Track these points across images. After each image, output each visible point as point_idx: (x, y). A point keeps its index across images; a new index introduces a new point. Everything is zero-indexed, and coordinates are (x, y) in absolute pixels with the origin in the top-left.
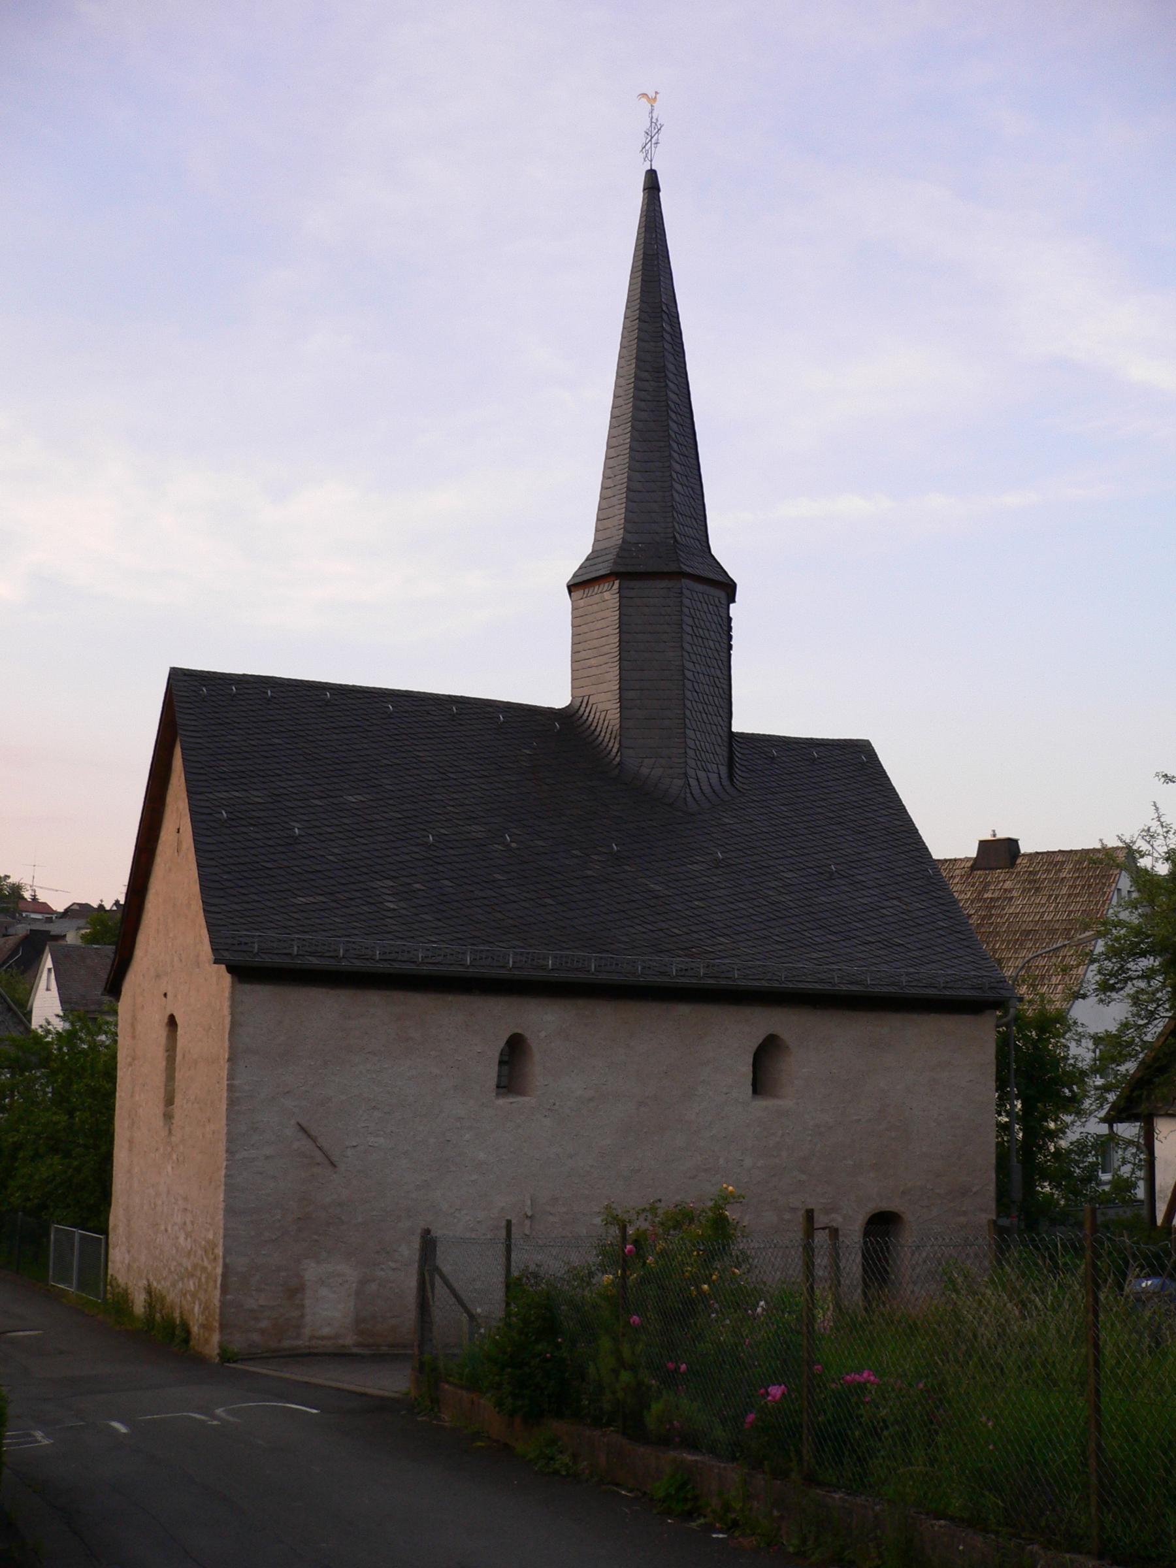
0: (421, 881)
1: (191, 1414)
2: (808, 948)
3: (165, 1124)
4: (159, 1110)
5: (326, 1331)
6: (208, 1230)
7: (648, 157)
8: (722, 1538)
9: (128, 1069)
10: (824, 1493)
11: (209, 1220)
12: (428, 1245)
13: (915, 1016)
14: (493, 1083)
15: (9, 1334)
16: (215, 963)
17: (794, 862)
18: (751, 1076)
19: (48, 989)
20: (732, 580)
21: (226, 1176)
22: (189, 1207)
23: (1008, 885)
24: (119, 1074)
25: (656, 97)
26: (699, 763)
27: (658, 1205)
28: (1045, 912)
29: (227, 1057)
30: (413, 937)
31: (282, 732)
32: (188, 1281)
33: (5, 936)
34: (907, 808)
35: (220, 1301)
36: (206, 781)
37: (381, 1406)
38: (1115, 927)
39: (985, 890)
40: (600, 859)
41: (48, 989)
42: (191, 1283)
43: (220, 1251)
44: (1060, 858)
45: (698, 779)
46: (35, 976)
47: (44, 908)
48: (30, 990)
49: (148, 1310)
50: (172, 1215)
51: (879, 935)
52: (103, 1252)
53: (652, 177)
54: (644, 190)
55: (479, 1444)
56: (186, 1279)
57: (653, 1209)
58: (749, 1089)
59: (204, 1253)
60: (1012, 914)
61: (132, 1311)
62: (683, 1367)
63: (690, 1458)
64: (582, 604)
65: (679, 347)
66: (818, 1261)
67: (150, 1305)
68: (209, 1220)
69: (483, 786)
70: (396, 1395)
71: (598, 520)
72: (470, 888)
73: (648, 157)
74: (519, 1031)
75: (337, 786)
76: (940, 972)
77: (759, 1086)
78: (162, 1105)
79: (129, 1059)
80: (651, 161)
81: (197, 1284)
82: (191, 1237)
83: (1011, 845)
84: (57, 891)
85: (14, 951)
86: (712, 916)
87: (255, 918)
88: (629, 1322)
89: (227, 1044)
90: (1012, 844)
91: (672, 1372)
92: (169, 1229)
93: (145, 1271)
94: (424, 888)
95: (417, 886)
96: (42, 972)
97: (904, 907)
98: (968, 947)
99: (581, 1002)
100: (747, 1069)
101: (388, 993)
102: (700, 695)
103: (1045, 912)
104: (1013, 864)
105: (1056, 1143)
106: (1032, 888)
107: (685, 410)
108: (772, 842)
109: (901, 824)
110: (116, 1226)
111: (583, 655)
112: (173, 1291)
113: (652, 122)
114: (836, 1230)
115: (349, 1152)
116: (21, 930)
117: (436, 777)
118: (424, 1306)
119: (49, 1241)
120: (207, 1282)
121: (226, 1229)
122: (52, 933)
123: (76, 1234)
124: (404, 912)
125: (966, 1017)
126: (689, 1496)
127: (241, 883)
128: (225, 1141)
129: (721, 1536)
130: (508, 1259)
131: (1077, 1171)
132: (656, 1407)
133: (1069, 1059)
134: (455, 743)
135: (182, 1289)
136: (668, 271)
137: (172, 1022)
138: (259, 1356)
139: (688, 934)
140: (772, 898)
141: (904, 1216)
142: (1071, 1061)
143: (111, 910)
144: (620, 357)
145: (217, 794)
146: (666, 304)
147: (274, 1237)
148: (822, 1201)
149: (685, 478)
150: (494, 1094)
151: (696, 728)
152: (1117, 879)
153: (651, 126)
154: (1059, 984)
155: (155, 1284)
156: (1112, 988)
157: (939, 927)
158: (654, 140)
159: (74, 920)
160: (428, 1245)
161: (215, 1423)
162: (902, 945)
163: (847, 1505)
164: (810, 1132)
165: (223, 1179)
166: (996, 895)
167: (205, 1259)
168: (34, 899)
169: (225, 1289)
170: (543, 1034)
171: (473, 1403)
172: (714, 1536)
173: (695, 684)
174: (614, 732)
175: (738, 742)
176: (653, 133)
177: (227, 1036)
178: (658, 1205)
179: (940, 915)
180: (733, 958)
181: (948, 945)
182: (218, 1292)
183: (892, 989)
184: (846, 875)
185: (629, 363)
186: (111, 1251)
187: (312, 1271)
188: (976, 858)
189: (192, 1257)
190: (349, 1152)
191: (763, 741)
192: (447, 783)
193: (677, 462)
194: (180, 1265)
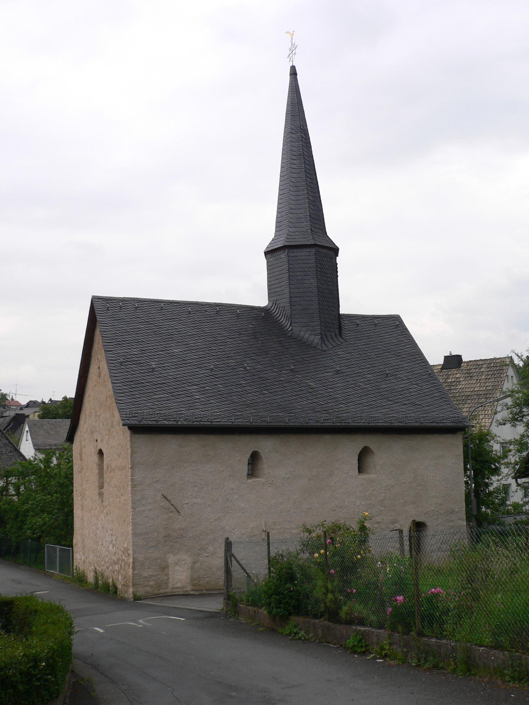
0: (209, 385)
1: (128, 623)
2: (379, 408)
3: (99, 497)
4: (96, 492)
5: (179, 585)
6: (124, 543)
7: (291, 60)
8: (381, 662)
9: (79, 474)
10: (427, 639)
11: (124, 539)
12: (228, 544)
13: (428, 436)
14: (246, 472)
15: (36, 593)
16: (123, 426)
17: (370, 370)
18: (358, 465)
19: (27, 440)
20: (337, 247)
21: (132, 519)
22: (114, 533)
23: (458, 376)
24: (75, 476)
25: (293, 34)
26: (326, 328)
27: (325, 523)
28: (475, 387)
29: (130, 467)
30: (208, 411)
31: (143, 322)
32: (115, 566)
33: (2, 417)
34: (418, 344)
35: (132, 574)
36: (112, 345)
37: (212, 615)
38: (517, 393)
39: (448, 378)
40: (286, 372)
41: (27, 440)
42: (117, 566)
43: (131, 552)
44: (481, 363)
45: (326, 336)
46: (21, 434)
47: (17, 404)
48: (19, 440)
49: (95, 579)
50: (105, 537)
51: (410, 401)
52: (71, 555)
53: (293, 69)
54: (290, 75)
55: (260, 629)
56: (114, 565)
57: (323, 525)
58: (358, 472)
59: (122, 553)
60: (461, 388)
61: (87, 581)
62: (355, 591)
63: (363, 629)
64: (271, 260)
65: (309, 144)
66: (408, 543)
67: (96, 578)
68: (124, 539)
69: (232, 342)
70: (217, 611)
71: (276, 222)
72: (231, 388)
73: (291, 60)
74: (256, 450)
75: (169, 345)
76: (437, 416)
77: (361, 469)
78: (97, 489)
79: (79, 470)
80: (293, 62)
81: (120, 567)
82: (115, 546)
83: (458, 358)
84: (27, 396)
85: (9, 424)
86: (337, 395)
87: (139, 405)
88: (330, 573)
89: (130, 461)
90: (459, 357)
91: (349, 593)
92: (104, 544)
93: (93, 563)
94: (211, 389)
95: (208, 388)
96: (24, 433)
97: (420, 388)
98: (448, 404)
99: (282, 436)
100: (356, 462)
101: (199, 436)
102: (326, 298)
103: (475, 387)
104: (460, 366)
105: (488, 489)
106: (469, 376)
107: (312, 172)
108: (360, 362)
109: (416, 351)
110: (76, 544)
111: (273, 282)
112: (107, 571)
113: (292, 44)
114: (402, 530)
115: (185, 506)
116: (12, 414)
117: (212, 339)
118: (228, 572)
119: (44, 552)
120: (125, 566)
121: (133, 542)
122: (25, 415)
123: (58, 548)
124: (203, 400)
125: (449, 435)
126: (363, 645)
127: (131, 390)
128: (131, 503)
129: (381, 661)
130: (269, 549)
131: (497, 500)
132: (345, 608)
133: (493, 451)
134: (219, 324)
135: (112, 570)
136: (302, 110)
137: (101, 453)
138: (150, 597)
139: (326, 404)
140: (362, 386)
141: (426, 523)
142: (494, 453)
143: (48, 403)
144: (283, 150)
145: (117, 351)
146: (302, 125)
147: (154, 545)
148: (390, 518)
149: (314, 202)
150: (246, 478)
151: (324, 313)
152: (506, 371)
153: (292, 46)
154: (483, 419)
155: (98, 568)
156: (517, 420)
157: (435, 396)
158: (293, 52)
159: (33, 408)
160: (228, 544)
161: (141, 626)
162: (420, 404)
163: (438, 644)
164: (384, 488)
165: (131, 521)
166: (453, 380)
167: (123, 556)
168: (12, 399)
169: (134, 568)
170: (266, 451)
171: (255, 612)
172: (378, 661)
173: (323, 293)
174: (288, 316)
175: (342, 318)
176: (293, 49)
177: (129, 458)
178: (325, 523)
179: (435, 391)
180: (347, 414)
181: (440, 404)
182: (131, 570)
183: (417, 424)
184: (393, 375)
185: (287, 152)
186: (74, 554)
187: (171, 559)
188: (443, 364)
189: (117, 555)
190: (185, 506)
191: (353, 317)
192: (217, 342)
193: (310, 196)
194: (111, 559)
